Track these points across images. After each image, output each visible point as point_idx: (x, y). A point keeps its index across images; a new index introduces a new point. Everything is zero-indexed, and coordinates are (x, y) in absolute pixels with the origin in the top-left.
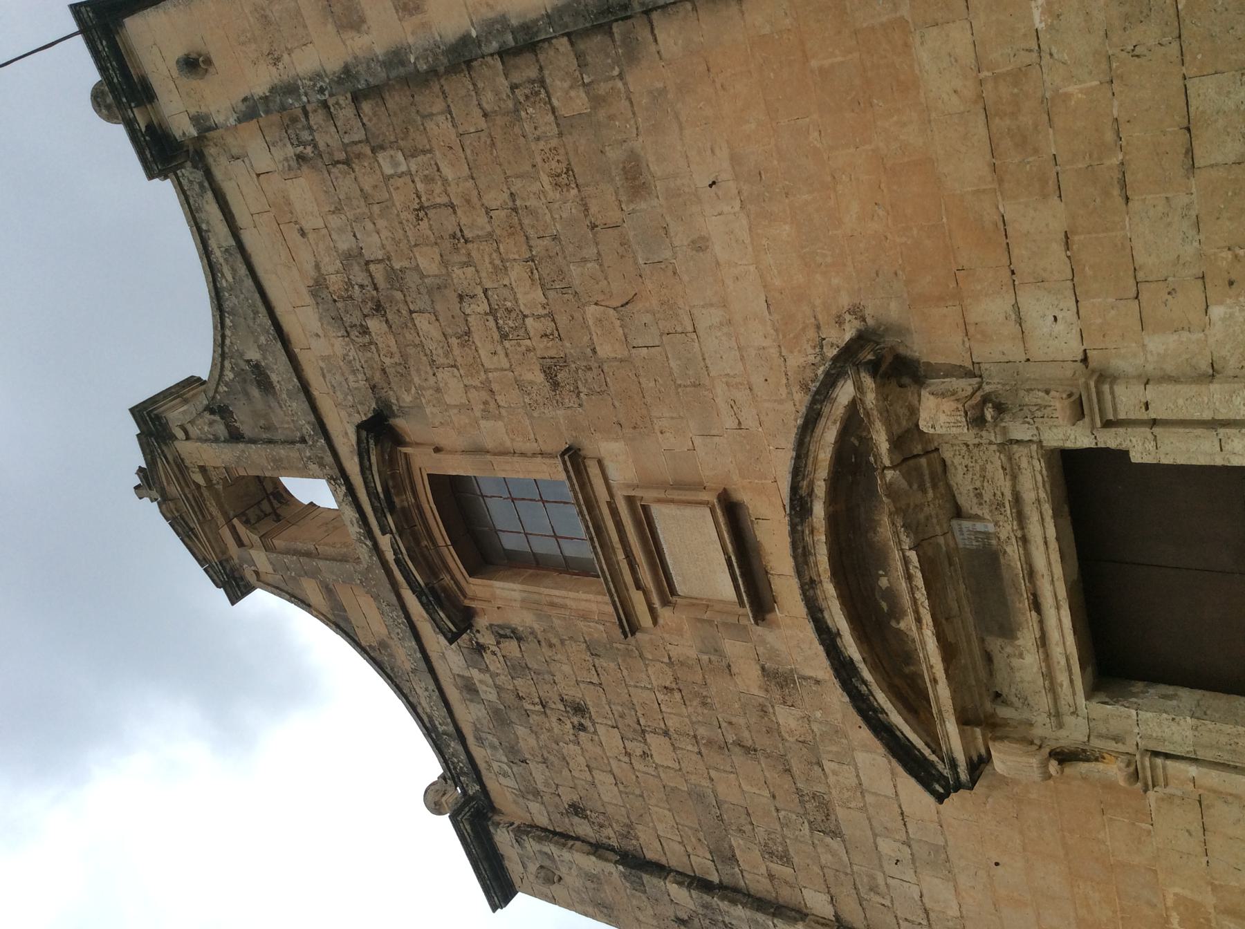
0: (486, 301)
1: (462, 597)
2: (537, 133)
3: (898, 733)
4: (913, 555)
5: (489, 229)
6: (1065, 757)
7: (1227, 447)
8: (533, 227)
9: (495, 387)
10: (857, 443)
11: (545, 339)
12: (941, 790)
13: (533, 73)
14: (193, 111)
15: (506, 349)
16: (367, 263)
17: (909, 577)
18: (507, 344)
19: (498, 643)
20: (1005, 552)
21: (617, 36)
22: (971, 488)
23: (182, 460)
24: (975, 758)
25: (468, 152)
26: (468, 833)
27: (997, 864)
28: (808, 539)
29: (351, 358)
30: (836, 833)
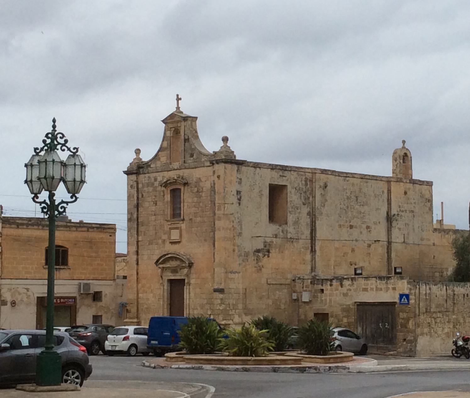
6: (161, 277)
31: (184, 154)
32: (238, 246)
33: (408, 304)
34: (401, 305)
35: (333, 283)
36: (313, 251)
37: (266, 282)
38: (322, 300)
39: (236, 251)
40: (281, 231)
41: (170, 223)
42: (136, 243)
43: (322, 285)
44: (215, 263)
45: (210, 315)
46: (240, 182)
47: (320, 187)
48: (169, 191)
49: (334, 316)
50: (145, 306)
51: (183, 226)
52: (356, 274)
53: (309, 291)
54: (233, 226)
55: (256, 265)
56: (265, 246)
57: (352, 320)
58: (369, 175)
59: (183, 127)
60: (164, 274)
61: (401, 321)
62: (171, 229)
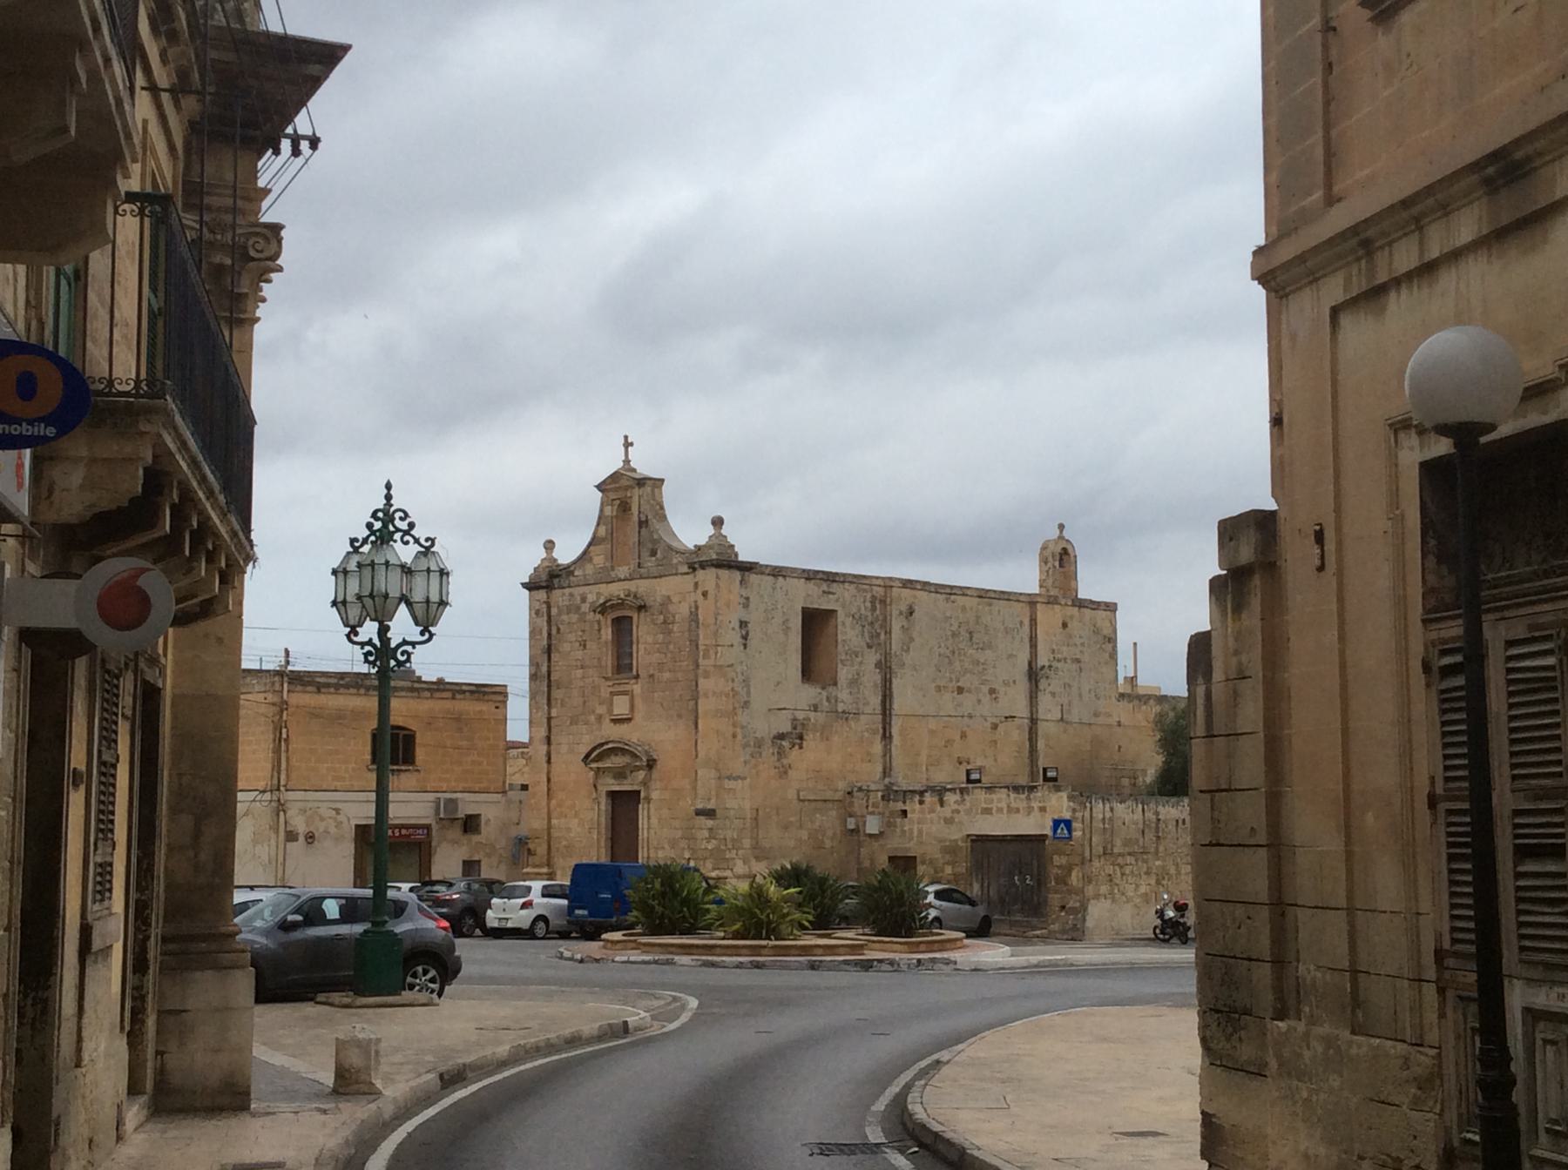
6: (595, 786)
31: (639, 551)
32: (742, 727)
33: (1070, 838)
34: (1056, 842)
36: (887, 737)
37: (796, 797)
38: (903, 832)
39: (739, 737)
40: (825, 698)
41: (611, 683)
42: (546, 720)
43: (904, 802)
45: (689, 859)
46: (746, 603)
47: (901, 613)
48: (609, 622)
50: (564, 843)
51: (637, 688)
52: (969, 781)
53: (879, 813)
54: (733, 689)
55: (777, 764)
56: (795, 728)
57: (962, 868)
58: (995, 591)
59: (636, 499)
60: (600, 781)
61: (1055, 871)
62: (612, 694)
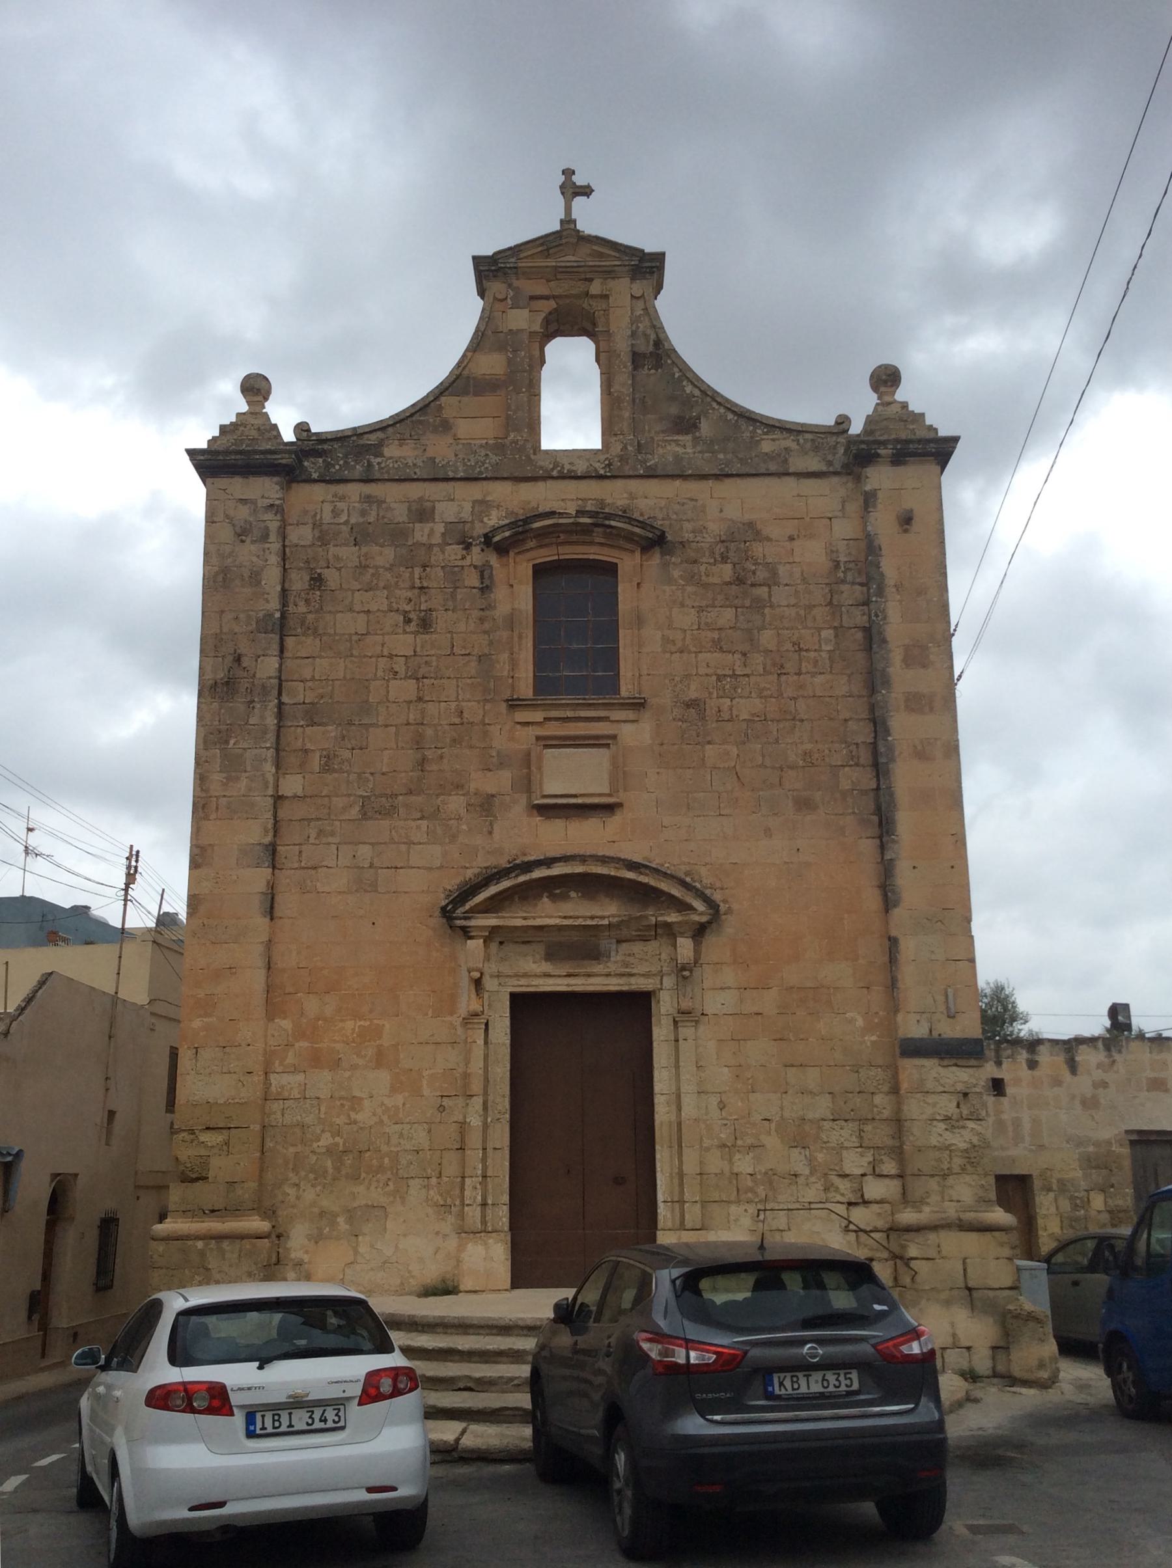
0: (742, 673)
1: (517, 551)
2: (833, 751)
3: (483, 889)
4: (606, 922)
5: (785, 695)
7: (663, 1070)
8: (784, 727)
9: (685, 656)
10: (662, 899)
11: (717, 710)
12: (448, 909)
13: (862, 761)
14: (880, 495)
15: (711, 676)
16: (770, 587)
17: (592, 918)
18: (714, 678)
19: (475, 567)
20: (600, 964)
21: (872, 817)
22: (634, 952)
23: (613, 278)
24: (468, 929)
25: (827, 699)
26: (276, 459)
27: (374, 924)
28: (613, 865)
29: (705, 535)
30: (365, 816)
35: (1037, 1058)
43: (999, 1063)
44: (896, 912)
45: (863, 1175)
49: (1055, 1187)
50: (326, 1140)
62: (548, 742)
